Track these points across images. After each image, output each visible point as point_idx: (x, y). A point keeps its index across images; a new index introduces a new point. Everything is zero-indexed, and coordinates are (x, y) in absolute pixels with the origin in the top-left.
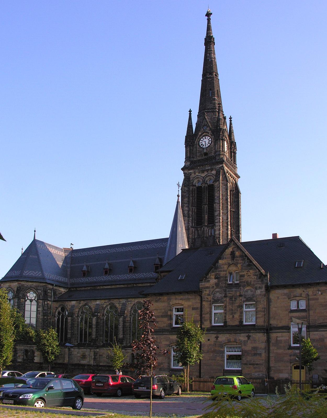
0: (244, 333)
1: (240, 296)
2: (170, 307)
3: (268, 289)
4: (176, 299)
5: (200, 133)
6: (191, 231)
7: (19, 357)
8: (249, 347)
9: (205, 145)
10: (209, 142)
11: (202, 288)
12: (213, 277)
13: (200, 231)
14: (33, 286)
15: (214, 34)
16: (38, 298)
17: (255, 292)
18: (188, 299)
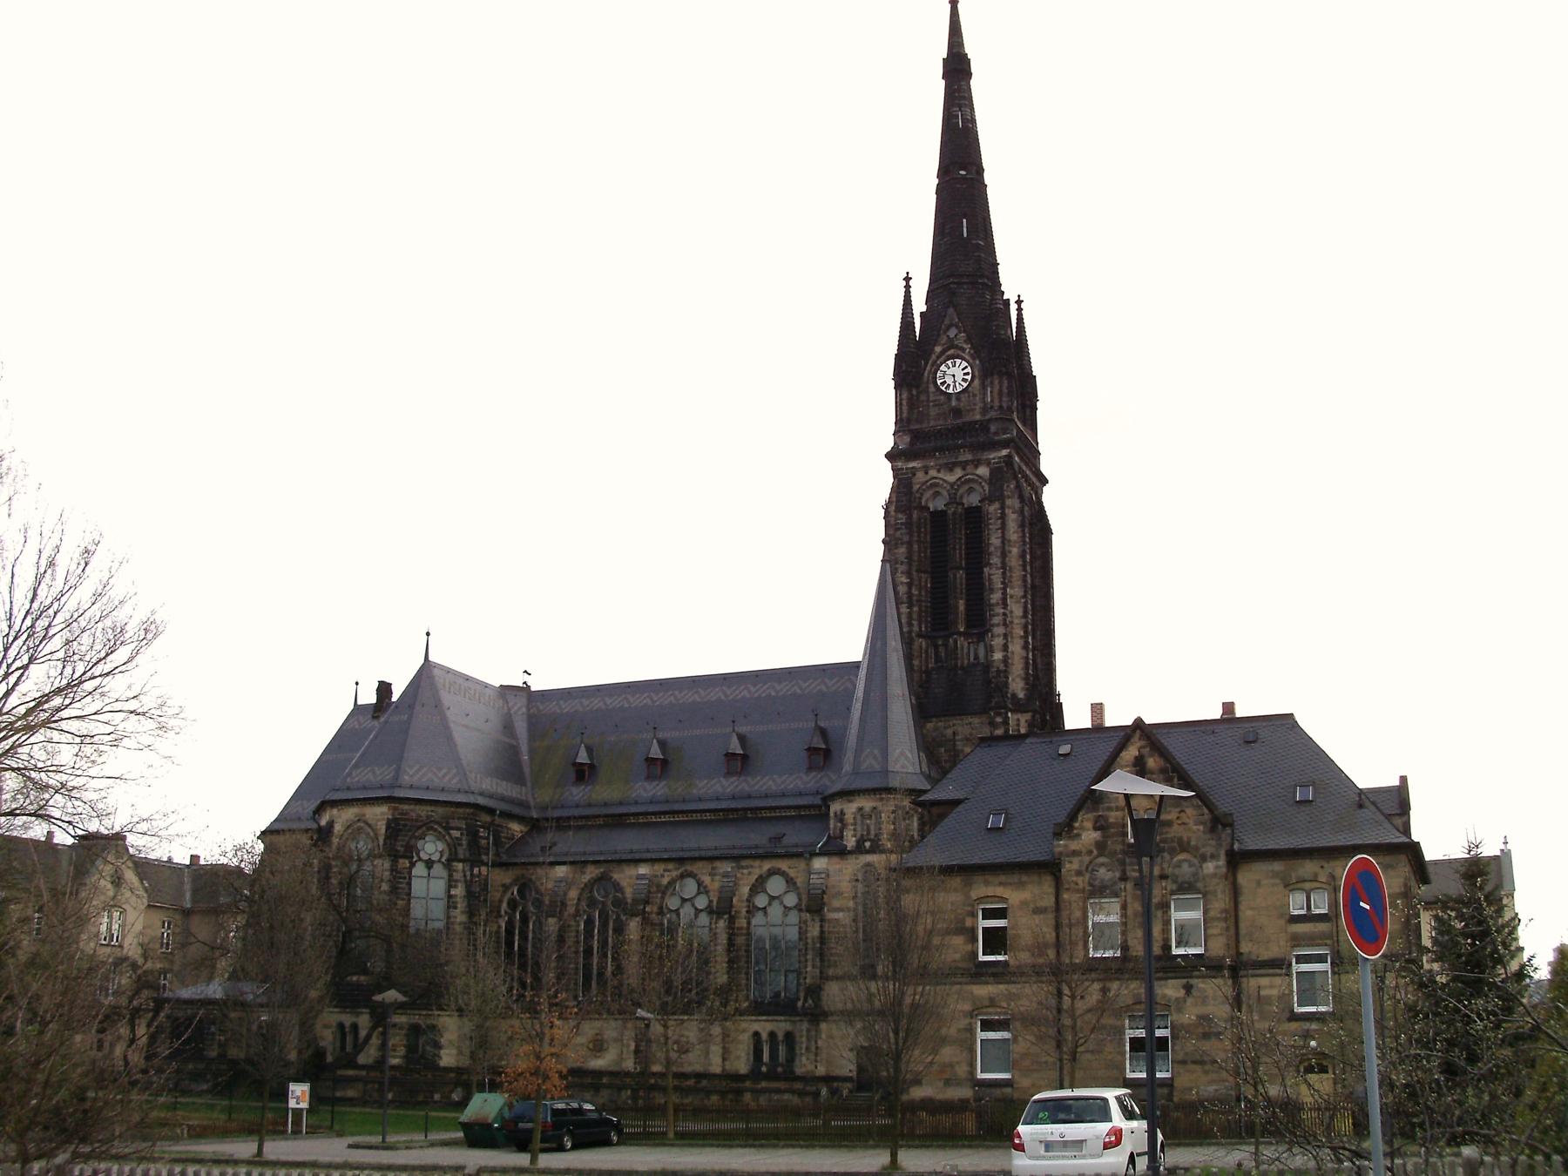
0: (1172, 978)
1: (1163, 877)
2: (969, 905)
3: (1237, 859)
4: (987, 883)
5: (938, 349)
6: (916, 646)
7: (395, 1050)
8: (1188, 1016)
9: (952, 385)
10: (966, 377)
11: (1061, 853)
12: (1089, 825)
13: (942, 650)
14: (436, 817)
15: (970, 48)
16: (450, 854)
17: (1201, 867)
18: (1021, 885)
